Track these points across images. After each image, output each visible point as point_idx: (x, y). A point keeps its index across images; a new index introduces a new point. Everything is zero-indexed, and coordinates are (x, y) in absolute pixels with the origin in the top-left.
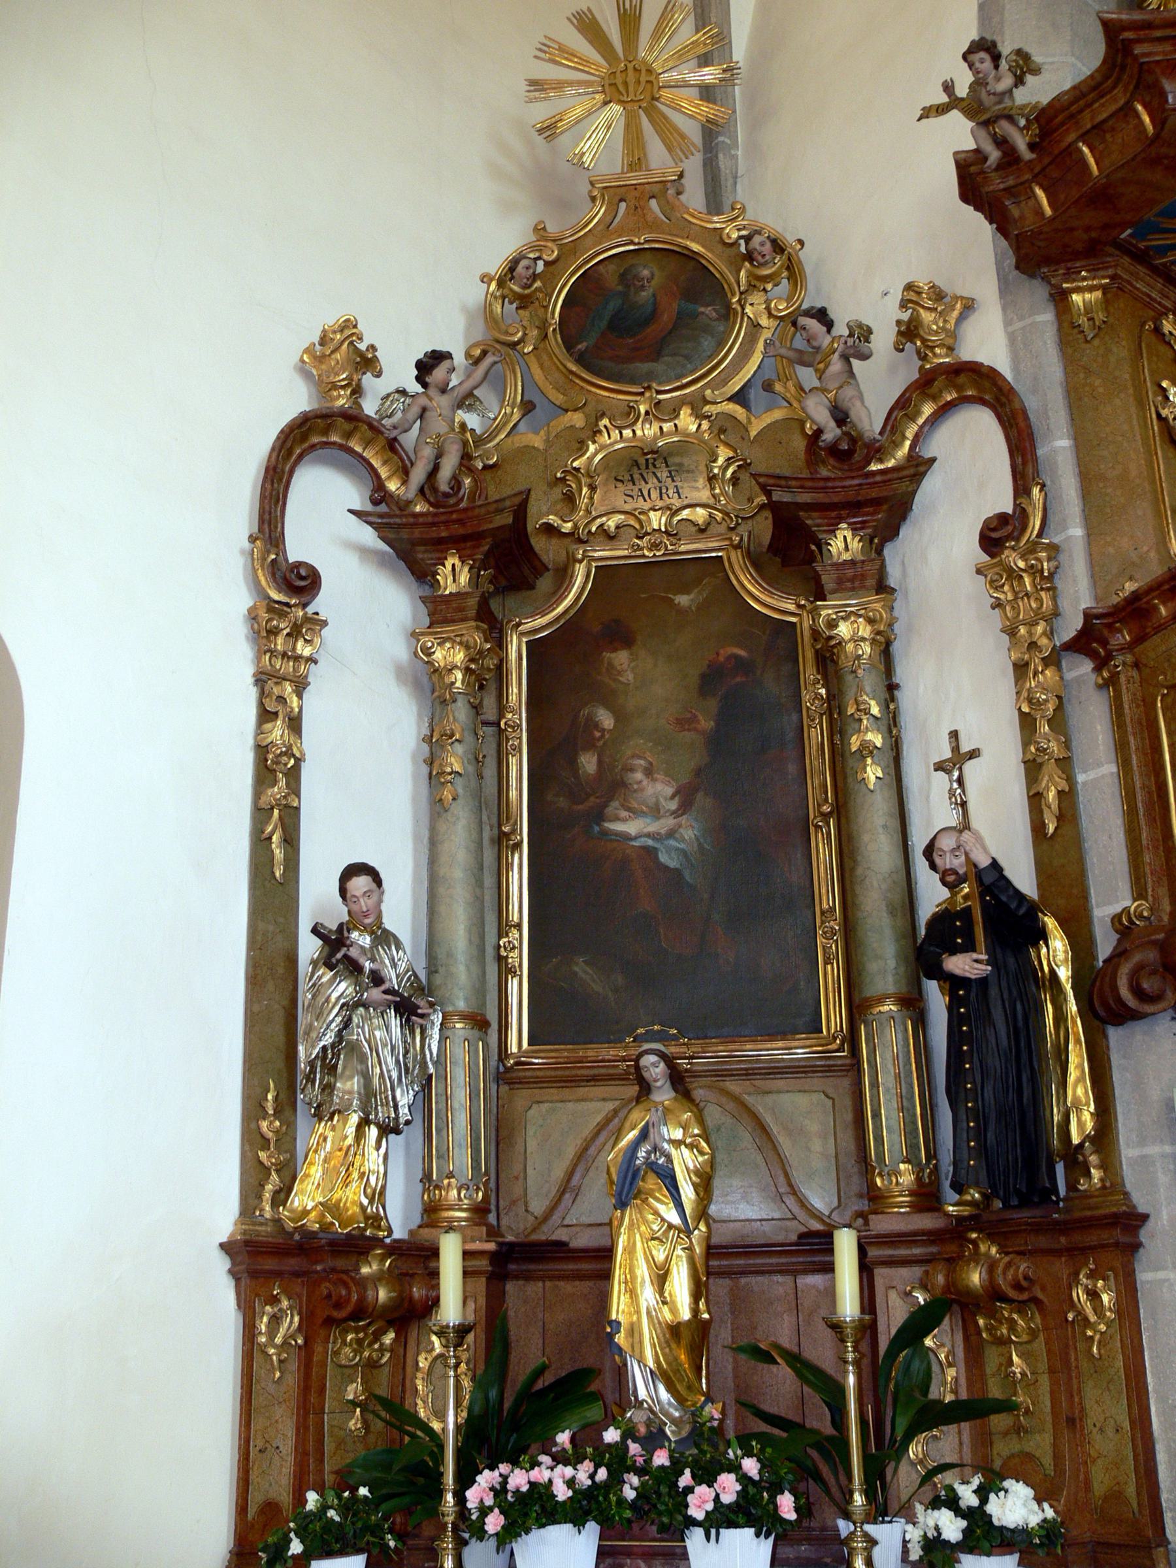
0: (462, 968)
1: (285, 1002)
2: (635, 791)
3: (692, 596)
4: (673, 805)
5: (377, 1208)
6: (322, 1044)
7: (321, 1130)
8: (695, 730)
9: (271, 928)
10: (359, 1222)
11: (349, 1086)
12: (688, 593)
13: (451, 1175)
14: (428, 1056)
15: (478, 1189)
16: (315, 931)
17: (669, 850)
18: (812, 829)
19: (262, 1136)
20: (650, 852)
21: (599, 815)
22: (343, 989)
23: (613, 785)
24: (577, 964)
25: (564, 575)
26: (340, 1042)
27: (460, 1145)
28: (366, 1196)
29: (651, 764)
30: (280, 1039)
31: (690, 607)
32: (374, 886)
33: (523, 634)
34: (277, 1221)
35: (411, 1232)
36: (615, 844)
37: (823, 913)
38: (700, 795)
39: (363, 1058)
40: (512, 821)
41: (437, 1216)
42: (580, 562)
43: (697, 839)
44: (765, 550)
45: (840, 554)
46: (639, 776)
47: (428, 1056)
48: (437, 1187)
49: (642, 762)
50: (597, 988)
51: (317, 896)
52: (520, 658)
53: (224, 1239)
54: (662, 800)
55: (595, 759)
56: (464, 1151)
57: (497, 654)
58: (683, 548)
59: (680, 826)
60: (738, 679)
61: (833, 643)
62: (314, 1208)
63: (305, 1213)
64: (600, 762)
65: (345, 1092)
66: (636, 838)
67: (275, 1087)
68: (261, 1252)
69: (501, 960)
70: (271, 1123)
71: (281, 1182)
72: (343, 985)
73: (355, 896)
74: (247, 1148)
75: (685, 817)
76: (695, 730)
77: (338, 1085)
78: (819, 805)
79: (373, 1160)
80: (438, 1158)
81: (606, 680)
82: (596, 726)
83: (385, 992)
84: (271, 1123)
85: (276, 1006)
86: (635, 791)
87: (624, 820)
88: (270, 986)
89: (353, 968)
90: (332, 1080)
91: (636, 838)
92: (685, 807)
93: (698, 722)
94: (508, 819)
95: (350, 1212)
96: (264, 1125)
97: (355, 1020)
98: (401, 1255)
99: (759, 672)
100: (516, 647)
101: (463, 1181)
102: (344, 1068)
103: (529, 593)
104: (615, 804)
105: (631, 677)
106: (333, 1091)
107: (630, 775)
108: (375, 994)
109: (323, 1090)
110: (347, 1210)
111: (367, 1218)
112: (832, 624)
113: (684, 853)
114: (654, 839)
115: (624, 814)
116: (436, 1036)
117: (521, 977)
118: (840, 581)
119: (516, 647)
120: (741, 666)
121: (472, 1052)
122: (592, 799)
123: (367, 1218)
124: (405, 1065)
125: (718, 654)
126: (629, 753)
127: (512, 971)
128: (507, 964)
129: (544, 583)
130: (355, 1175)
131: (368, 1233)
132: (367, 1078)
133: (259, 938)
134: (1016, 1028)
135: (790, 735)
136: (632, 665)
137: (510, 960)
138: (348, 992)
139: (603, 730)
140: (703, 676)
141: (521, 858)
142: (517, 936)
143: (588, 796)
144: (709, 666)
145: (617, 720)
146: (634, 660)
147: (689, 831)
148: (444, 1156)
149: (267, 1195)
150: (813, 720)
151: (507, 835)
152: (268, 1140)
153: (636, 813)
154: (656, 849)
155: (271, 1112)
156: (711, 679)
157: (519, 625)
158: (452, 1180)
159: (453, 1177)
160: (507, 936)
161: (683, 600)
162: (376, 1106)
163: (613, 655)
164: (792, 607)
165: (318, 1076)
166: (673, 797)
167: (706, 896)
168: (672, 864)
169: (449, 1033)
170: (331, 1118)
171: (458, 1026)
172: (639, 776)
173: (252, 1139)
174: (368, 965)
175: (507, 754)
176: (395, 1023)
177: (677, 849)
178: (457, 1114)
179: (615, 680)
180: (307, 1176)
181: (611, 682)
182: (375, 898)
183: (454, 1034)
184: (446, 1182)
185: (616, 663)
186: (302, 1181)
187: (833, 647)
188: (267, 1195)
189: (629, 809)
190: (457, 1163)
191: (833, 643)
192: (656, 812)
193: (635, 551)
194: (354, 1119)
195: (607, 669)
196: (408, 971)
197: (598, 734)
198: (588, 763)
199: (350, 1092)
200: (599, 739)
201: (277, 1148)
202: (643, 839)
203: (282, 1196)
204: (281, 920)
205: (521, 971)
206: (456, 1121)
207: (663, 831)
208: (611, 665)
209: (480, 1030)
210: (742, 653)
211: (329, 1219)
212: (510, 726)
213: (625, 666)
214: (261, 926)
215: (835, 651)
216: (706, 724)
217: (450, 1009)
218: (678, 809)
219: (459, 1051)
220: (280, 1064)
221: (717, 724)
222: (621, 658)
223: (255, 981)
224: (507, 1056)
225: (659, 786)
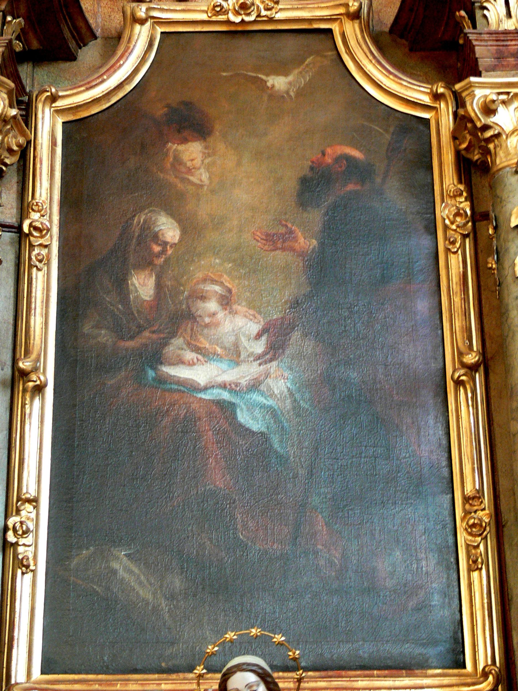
2: (207, 326)
3: (290, 78)
4: (259, 347)
8: (292, 249)
12: (286, 75)
17: (251, 407)
18: (450, 385)
20: (226, 409)
21: (155, 357)
23: (177, 317)
24: (117, 558)
25: (115, 42)
29: (230, 291)
31: (287, 93)
33: (59, 112)
36: (176, 396)
37: (466, 499)
38: (296, 335)
40: (34, 356)
42: (142, 22)
43: (291, 394)
44: (387, 30)
45: (500, 21)
46: (212, 306)
49: (217, 288)
50: (146, 593)
52: (54, 143)
54: (243, 339)
55: (151, 282)
57: (23, 134)
58: (280, 16)
59: (267, 375)
60: (351, 187)
61: (489, 134)
64: (159, 286)
66: (205, 389)
75: (274, 363)
76: (292, 249)
78: (461, 354)
81: (171, 178)
82: (156, 237)
86: (207, 326)
87: (191, 364)
91: (205, 389)
92: (275, 350)
93: (295, 239)
94: (27, 353)
99: (378, 180)
100: (48, 127)
103: (68, 64)
104: (178, 341)
105: (205, 177)
107: (200, 304)
112: (489, 110)
113: (273, 412)
114: (231, 391)
115: (189, 355)
118: (500, 56)
119: (48, 127)
120: (353, 169)
122: (146, 334)
125: (324, 154)
126: (200, 275)
128: (16, 555)
129: (89, 54)
134: (112, 681)
135: (423, 262)
136: (207, 161)
137: (21, 549)
139: (165, 243)
140: (304, 181)
141: (42, 408)
142: (33, 515)
143: (141, 329)
144: (312, 168)
145: (184, 231)
146: (209, 155)
147: (281, 382)
150: (453, 243)
151: (24, 374)
153: (206, 355)
154: (233, 406)
156: (313, 185)
157: (54, 98)
160: (18, 512)
161: (279, 82)
163: (181, 148)
164: (426, 99)
166: (258, 336)
167: (302, 472)
168: (256, 426)
172: (212, 306)
175: (31, 266)
177: (263, 407)
179: (184, 180)
181: (177, 181)
185: (185, 157)
187: (488, 140)
189: (197, 350)
191: (489, 134)
192: (235, 355)
193: (218, 13)
195: (173, 165)
197: (157, 249)
198: (143, 286)
200: (158, 255)
202: (216, 391)
207: (244, 382)
208: (178, 161)
210: (356, 153)
212: (36, 228)
213: (198, 162)
215: (491, 146)
216: (306, 242)
218: (265, 354)
221: (322, 244)
222: (192, 151)
225: (240, 321)
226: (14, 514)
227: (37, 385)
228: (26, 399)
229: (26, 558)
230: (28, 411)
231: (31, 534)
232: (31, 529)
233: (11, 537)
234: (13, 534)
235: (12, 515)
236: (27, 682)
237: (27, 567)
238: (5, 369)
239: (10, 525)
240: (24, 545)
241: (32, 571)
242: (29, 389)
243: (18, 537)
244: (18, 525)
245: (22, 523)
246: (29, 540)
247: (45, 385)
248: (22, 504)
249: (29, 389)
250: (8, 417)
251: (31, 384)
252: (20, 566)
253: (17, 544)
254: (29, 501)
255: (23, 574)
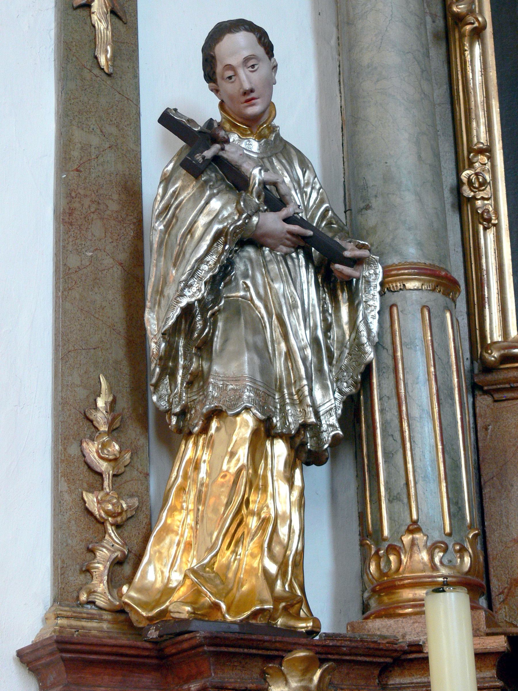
0: (409, 197)
1: (122, 256)
5: (291, 586)
6: (184, 302)
7: (190, 454)
9: (95, 140)
10: (262, 602)
11: (232, 368)
13: (414, 528)
14: (364, 333)
15: (463, 550)
16: (168, 120)
19: (90, 468)
22: (217, 209)
26: (216, 301)
27: (425, 478)
28: (272, 557)
30: (116, 312)
32: (260, 51)
34: (121, 611)
35: (351, 625)
39: (256, 327)
41: (395, 598)
47: (364, 333)
48: (393, 549)
51: (170, 80)
53: (26, 640)
56: (433, 486)
62: (182, 584)
63: (168, 591)
65: (227, 379)
67: (111, 389)
68: (92, 662)
69: (461, 203)
70: (104, 445)
71: (125, 544)
72: (216, 204)
73: (230, 67)
74: (64, 486)
77: (216, 368)
79: (281, 498)
80: (390, 501)
83: (287, 220)
84: (104, 445)
85: (108, 261)
88: (97, 229)
89: (235, 180)
90: (205, 366)
95: (245, 588)
96: (92, 449)
97: (240, 266)
98: (340, 662)
101: (437, 536)
102: (225, 341)
106: (206, 382)
108: (272, 222)
109: (190, 384)
110: (241, 584)
111: (277, 600)
116: (376, 303)
117: (497, 226)
121: (435, 326)
123: (277, 600)
124: (328, 349)
127: (487, 221)
128: (474, 210)
130: (253, 522)
131: (280, 622)
132: (263, 354)
133: (76, 154)
138: (225, 213)
148: (401, 496)
149: (101, 568)
152: (100, 474)
155: (104, 428)
158: (417, 536)
159: (419, 530)
160: (471, 165)
162: (283, 405)
165: (181, 362)
169: (393, 298)
170: (205, 430)
171: (410, 285)
173: (72, 473)
174: (257, 175)
176: (306, 277)
178: (417, 426)
180: (167, 529)
182: (263, 68)
183: (405, 298)
184: (407, 539)
186: (160, 540)
188: (101, 568)
190: (423, 507)
194: (245, 425)
196: (322, 202)
199: (236, 379)
201: (114, 487)
203: (127, 569)
204: (113, 130)
205: (498, 218)
206: (417, 438)
209: (446, 294)
211: (209, 598)
214: (78, 135)
217: (395, 260)
219: (412, 325)
220: (118, 351)
223: (70, 218)
224: (486, 347)
226: (467, 167)
227: (476, 28)
228: (464, 45)
229: (486, 211)
230: (468, 58)
231: (489, 187)
232: (488, 181)
233: (467, 192)
234: (468, 189)
235: (464, 169)
236: (504, 342)
237: (489, 220)
238: (437, 22)
239: (465, 179)
240: (483, 199)
241: (494, 225)
242: (467, 33)
243: (475, 190)
244: (473, 178)
245: (477, 174)
246: (487, 192)
247: (484, 27)
248: (475, 156)
249: (467, 33)
250: (446, 71)
251: (468, 27)
252: (481, 221)
253: (474, 198)
254: (481, 151)
255: (485, 229)
